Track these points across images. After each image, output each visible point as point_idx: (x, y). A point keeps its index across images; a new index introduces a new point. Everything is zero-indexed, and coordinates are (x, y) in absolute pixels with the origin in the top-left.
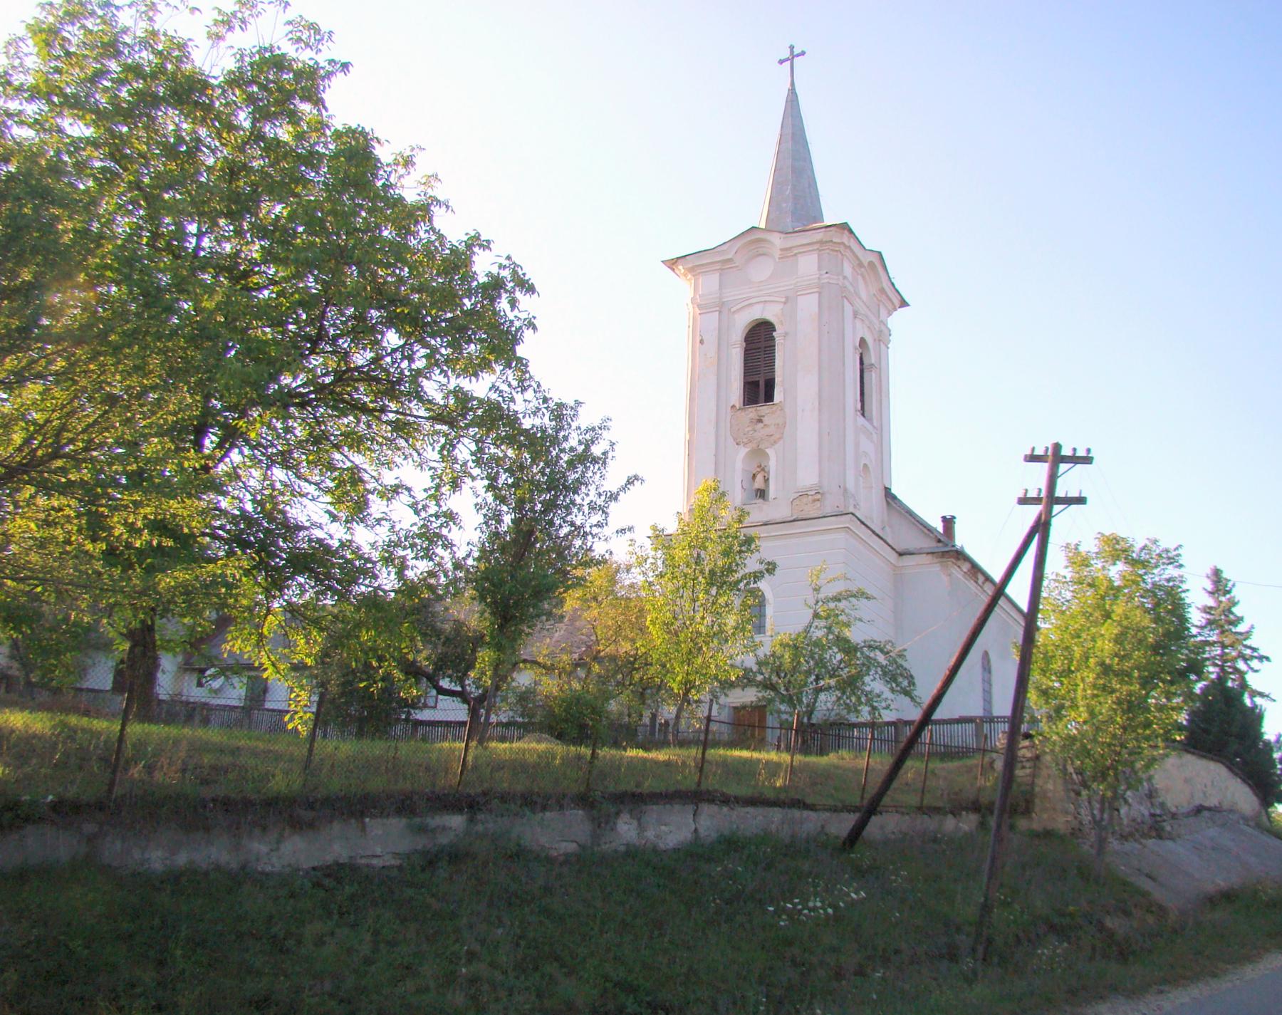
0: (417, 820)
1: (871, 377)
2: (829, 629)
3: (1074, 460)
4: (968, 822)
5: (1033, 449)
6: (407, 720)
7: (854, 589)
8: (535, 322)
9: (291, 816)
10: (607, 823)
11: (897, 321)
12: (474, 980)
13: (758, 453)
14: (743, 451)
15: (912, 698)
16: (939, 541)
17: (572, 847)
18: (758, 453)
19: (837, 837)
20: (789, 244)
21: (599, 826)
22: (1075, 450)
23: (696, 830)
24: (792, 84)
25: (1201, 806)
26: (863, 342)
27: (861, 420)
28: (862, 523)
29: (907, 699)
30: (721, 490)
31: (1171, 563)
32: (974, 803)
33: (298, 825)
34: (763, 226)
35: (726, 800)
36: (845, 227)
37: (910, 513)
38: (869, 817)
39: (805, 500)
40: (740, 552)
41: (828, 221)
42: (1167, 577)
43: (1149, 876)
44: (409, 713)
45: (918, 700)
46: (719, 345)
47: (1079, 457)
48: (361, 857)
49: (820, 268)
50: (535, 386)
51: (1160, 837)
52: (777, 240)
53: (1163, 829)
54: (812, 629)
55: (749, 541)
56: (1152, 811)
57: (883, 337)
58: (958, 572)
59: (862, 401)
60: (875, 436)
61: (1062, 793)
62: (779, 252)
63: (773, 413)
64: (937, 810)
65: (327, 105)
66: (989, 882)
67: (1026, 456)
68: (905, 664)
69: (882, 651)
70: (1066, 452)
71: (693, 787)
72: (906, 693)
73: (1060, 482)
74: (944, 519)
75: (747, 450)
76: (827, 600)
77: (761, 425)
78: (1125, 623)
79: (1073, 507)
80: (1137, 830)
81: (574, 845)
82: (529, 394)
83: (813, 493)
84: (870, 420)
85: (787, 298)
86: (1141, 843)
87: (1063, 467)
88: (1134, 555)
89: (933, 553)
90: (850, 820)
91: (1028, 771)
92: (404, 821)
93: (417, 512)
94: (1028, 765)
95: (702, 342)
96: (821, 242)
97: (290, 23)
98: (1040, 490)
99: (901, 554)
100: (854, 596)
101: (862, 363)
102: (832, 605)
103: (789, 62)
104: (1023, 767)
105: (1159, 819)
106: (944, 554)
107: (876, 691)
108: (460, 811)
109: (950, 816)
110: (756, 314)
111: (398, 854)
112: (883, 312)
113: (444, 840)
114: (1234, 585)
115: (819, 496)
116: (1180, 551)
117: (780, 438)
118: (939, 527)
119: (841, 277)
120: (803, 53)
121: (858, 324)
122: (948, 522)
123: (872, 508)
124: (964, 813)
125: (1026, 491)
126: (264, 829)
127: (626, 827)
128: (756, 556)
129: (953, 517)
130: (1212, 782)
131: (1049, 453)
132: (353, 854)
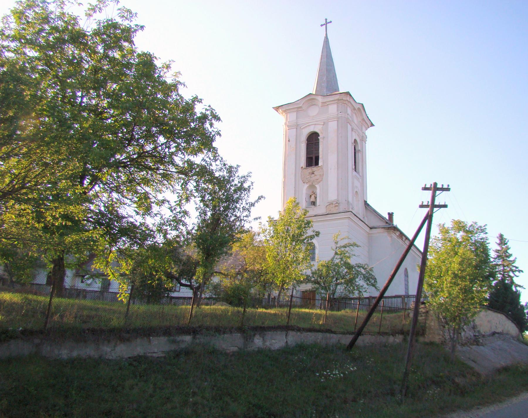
0: (172, 338)
1: (359, 155)
2: (342, 259)
3: (442, 189)
4: (399, 339)
5: (426, 185)
8: (221, 132)
9: (120, 336)
10: (250, 339)
12: (195, 404)
13: (312, 187)
14: (306, 186)
15: (376, 288)
16: (387, 223)
17: (235, 349)
18: (312, 187)
19: (345, 345)
20: (325, 100)
21: (247, 340)
22: (443, 185)
23: (287, 342)
24: (326, 34)
26: (355, 141)
27: (354, 173)
28: (355, 215)
29: (374, 288)
30: (297, 202)
31: (482, 232)
33: (123, 340)
34: (314, 93)
35: (299, 330)
36: (348, 94)
37: (375, 211)
38: (358, 337)
39: (331, 206)
40: (305, 227)
41: (341, 91)
42: (481, 237)
43: (473, 361)
45: (378, 288)
48: (149, 353)
49: (338, 111)
50: (220, 159)
51: (478, 345)
52: (320, 99)
53: (479, 341)
54: (335, 259)
55: (308, 223)
56: (475, 334)
57: (364, 139)
58: (395, 235)
60: (360, 179)
61: (438, 327)
66: (407, 363)
68: (373, 274)
69: (363, 268)
70: (439, 186)
71: (286, 324)
72: (373, 285)
73: (436, 198)
74: (389, 214)
75: (308, 185)
76: (341, 247)
77: (313, 175)
78: (463, 257)
79: (442, 209)
80: (468, 342)
81: (237, 348)
82: (218, 162)
83: (335, 203)
84: (358, 173)
86: (470, 347)
87: (438, 192)
88: (467, 229)
89: (384, 228)
90: (350, 338)
91: (423, 318)
93: (172, 211)
94: (423, 315)
95: (289, 141)
96: (338, 100)
98: (428, 202)
99: (371, 228)
102: (343, 249)
103: (325, 26)
104: (422, 316)
105: (477, 337)
106: (389, 228)
107: (361, 285)
108: (190, 334)
109: (391, 336)
110: (312, 129)
111: (164, 352)
112: (364, 128)
113: (183, 346)
114: (508, 241)
115: (337, 204)
116: (486, 227)
117: (321, 181)
118: (387, 217)
119: (346, 114)
120: (331, 22)
121: (354, 133)
122: (391, 215)
123: (359, 209)
124: (397, 335)
125: (423, 202)
127: (258, 341)
128: (311, 229)
129: (393, 213)
131: (432, 187)
132: (145, 352)
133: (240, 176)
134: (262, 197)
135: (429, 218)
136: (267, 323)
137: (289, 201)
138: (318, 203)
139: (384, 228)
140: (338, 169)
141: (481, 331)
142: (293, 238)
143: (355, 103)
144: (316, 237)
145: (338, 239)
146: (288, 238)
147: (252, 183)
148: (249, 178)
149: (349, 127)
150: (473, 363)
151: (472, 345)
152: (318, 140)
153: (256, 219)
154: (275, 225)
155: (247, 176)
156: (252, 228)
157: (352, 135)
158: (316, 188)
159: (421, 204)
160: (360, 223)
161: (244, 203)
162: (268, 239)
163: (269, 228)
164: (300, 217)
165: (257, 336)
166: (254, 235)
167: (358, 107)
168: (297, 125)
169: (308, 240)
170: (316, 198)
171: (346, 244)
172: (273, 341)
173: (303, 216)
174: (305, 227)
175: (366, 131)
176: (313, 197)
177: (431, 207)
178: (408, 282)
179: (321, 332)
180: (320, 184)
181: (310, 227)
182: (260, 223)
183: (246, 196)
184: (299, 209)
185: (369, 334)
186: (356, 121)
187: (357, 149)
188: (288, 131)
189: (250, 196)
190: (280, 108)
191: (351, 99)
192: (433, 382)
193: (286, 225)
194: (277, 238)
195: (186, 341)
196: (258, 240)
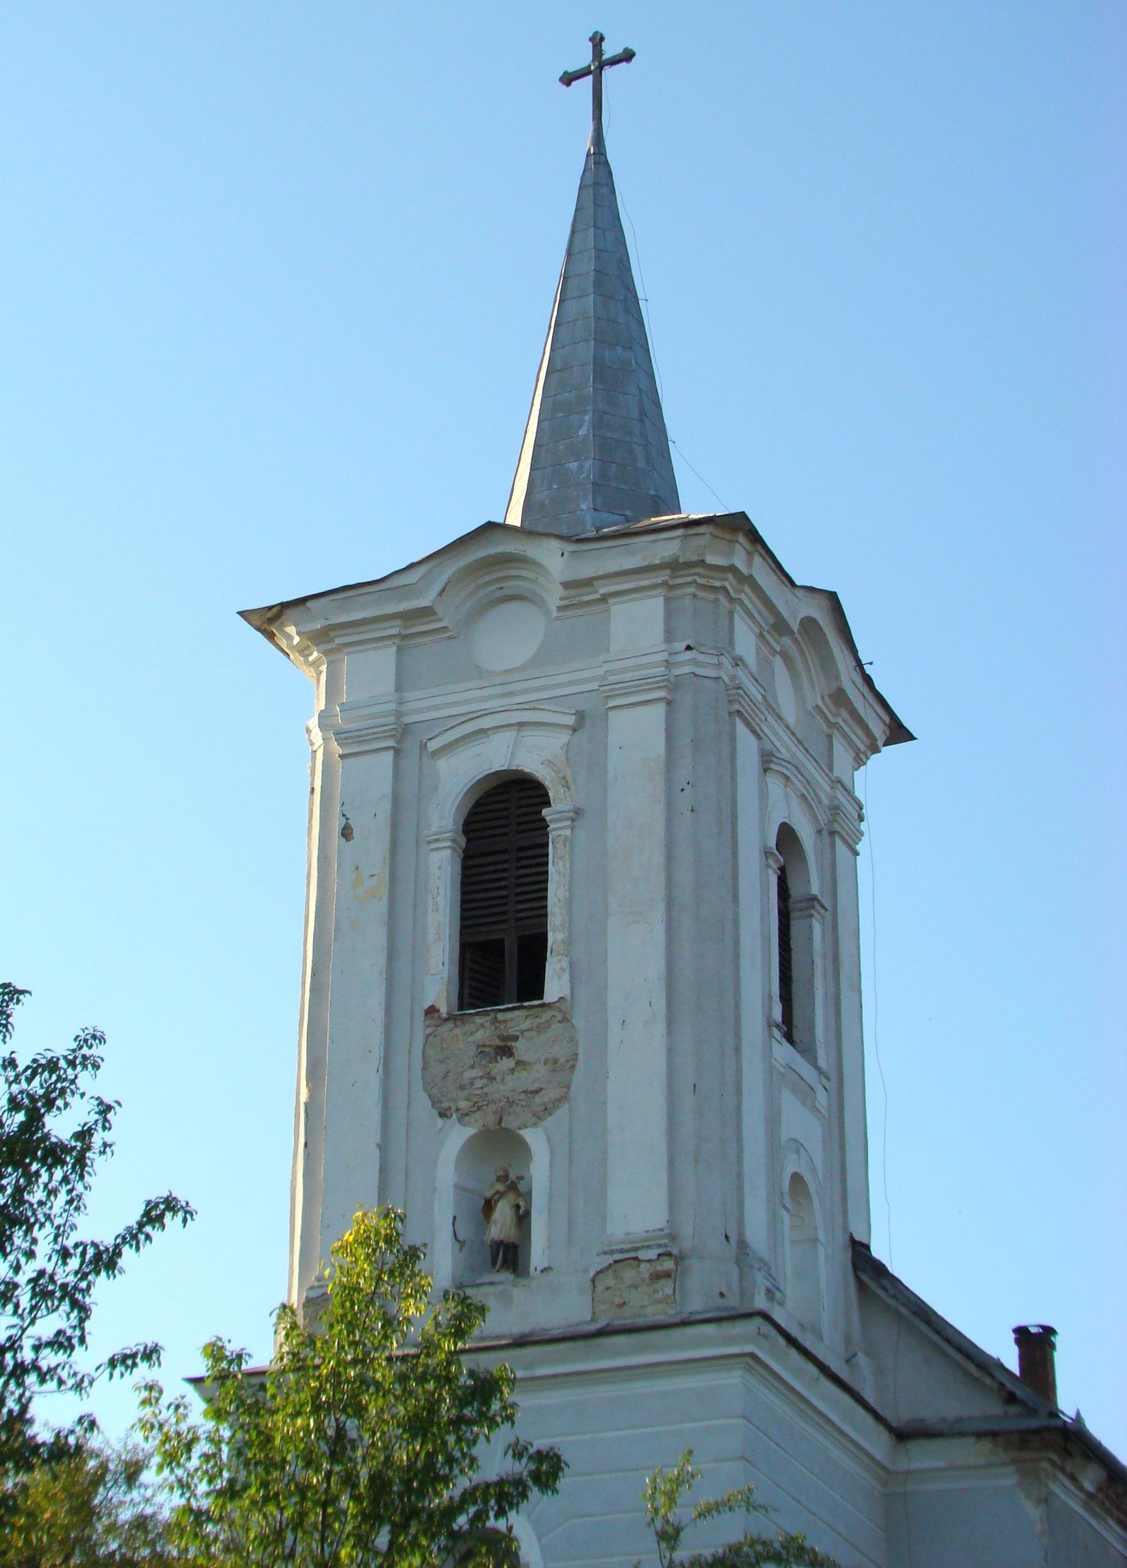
14: (458, 1135)
20: (587, 568)
26: (787, 836)
27: (783, 1051)
28: (792, 1341)
34: (514, 519)
39: (629, 1274)
40: (459, 1421)
41: (693, 508)
49: (669, 636)
60: (821, 1095)
62: (560, 591)
63: (540, 1029)
74: (1022, 1335)
75: (470, 1131)
77: (507, 1063)
83: (652, 1254)
84: (808, 1052)
85: (581, 716)
89: (993, 1435)
95: (346, 833)
96: (674, 566)
99: (902, 1435)
103: (589, 80)
112: (842, 755)
115: (668, 1264)
118: (1010, 1358)
119: (726, 661)
120: (628, 56)
121: (774, 785)
128: (503, 1435)
129: (1049, 1331)
133: (23, 1062)
134: (171, 1204)
137: (349, 1237)
138: (538, 1254)
139: (993, 1435)
140: (670, 1022)
142: (375, 1502)
143: (787, 591)
144: (534, 1493)
145: (683, 1513)
146: (345, 1501)
147: (105, 1109)
148: (84, 1079)
149: (747, 745)
152: (543, 825)
153: (123, 1361)
154: (255, 1409)
155: (72, 1063)
156: (93, 1424)
157: (763, 793)
158: (522, 1149)
160: (826, 1397)
161: (44, 1247)
162: (205, 1503)
163: (211, 1425)
164: (429, 1346)
166: (98, 1479)
167: (801, 615)
168: (403, 731)
169: (480, 1516)
170: (523, 1218)
173: (448, 1345)
174: (459, 1421)
175: (859, 775)
176: (503, 1211)
180: (549, 1121)
181: (493, 1423)
182: (150, 1388)
183: (63, 1197)
184: (420, 1290)
186: (789, 709)
187: (796, 890)
188: (340, 763)
189: (88, 1198)
190: (290, 613)
191: (757, 560)
193: (330, 1407)
194: (266, 1499)
196: (125, 1515)
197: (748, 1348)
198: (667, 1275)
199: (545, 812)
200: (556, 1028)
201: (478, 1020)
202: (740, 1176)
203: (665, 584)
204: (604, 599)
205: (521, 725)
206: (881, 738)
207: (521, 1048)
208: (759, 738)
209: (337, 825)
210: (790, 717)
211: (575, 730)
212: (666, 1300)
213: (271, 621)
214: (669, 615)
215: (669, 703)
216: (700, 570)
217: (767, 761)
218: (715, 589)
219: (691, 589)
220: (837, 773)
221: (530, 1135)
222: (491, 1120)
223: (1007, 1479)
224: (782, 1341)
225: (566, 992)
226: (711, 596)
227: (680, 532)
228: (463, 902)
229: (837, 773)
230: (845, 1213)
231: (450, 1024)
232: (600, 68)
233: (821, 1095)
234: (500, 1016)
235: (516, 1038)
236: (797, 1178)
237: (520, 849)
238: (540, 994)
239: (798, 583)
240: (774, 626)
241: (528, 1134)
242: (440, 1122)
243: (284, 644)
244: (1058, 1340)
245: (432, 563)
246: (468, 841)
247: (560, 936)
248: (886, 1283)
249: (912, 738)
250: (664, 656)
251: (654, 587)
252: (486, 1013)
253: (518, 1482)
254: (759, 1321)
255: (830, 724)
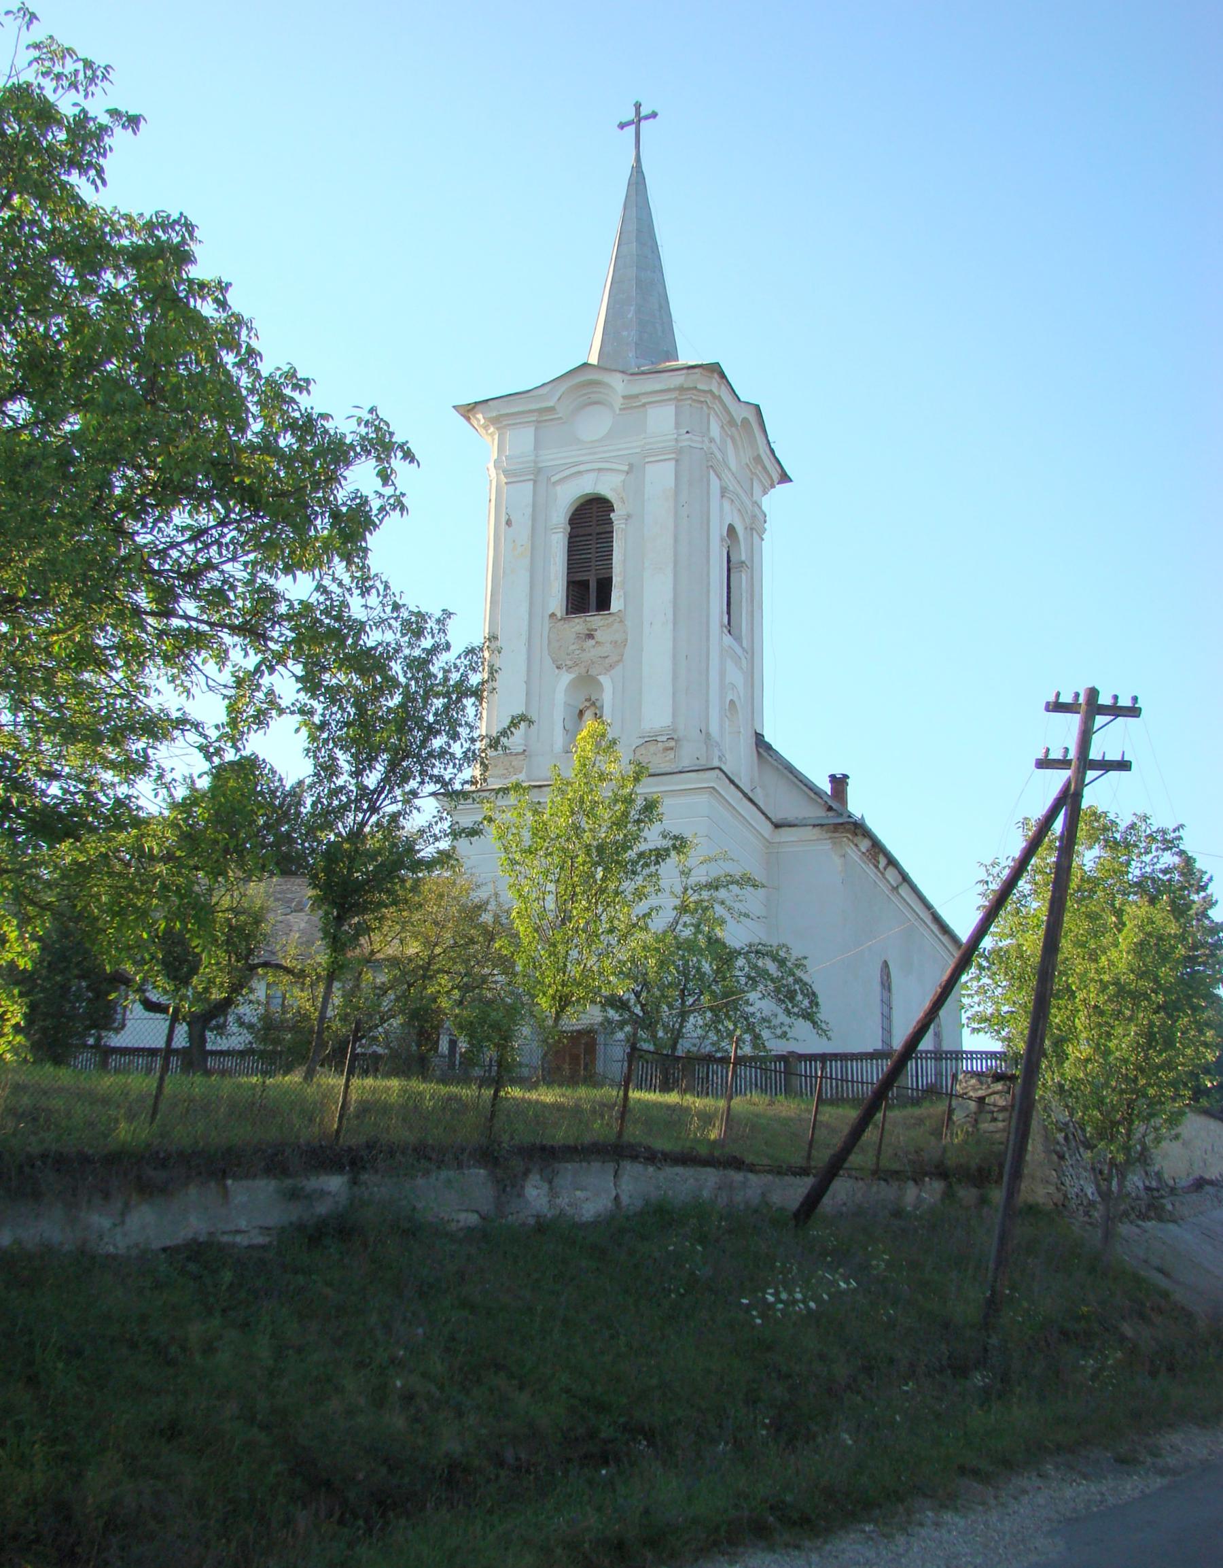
0: (289, 1182)
1: (741, 579)
2: (697, 926)
3: (1115, 711)
4: (933, 1190)
5: (1058, 695)
6: (96, 1046)
7: (737, 871)
8: (404, 500)
9: (139, 1178)
10: (513, 1186)
11: (775, 501)
12: (408, 1397)
13: (587, 681)
14: (566, 678)
15: (814, 1023)
16: (830, 809)
17: (473, 1219)
18: (587, 681)
19: (782, 1209)
20: (635, 389)
21: (504, 1191)
22: (1116, 697)
23: (617, 1197)
24: (638, 159)
25: (1201, 1178)
26: (731, 530)
27: (728, 639)
28: (732, 782)
29: (808, 1024)
30: (610, 736)
31: (1170, 848)
32: (937, 1167)
33: (147, 1190)
34: (594, 360)
35: (652, 1157)
36: (715, 370)
37: (790, 769)
38: (830, 1181)
39: (652, 748)
40: (638, 821)
41: (686, 358)
42: (1163, 867)
43: (1161, 1270)
44: (99, 1038)
45: (824, 1026)
46: (533, 529)
47: (1121, 708)
48: (224, 1233)
49: (677, 425)
50: (381, 588)
51: (1160, 1219)
52: (618, 384)
53: (1163, 1207)
54: (679, 927)
55: (650, 807)
56: (1147, 1183)
57: (757, 523)
58: (855, 852)
59: (729, 613)
60: (744, 661)
61: (1043, 1155)
62: (621, 400)
63: (609, 626)
64: (896, 1175)
65: (106, 176)
66: (996, 1269)
67: (1048, 704)
68: (805, 978)
69: (774, 959)
70: (1104, 699)
71: (612, 1138)
72: (808, 1016)
73: (1096, 739)
74: (833, 778)
75: (572, 676)
76: (699, 888)
77: (592, 642)
78: (1149, 929)
79: (1112, 774)
80: (1133, 1208)
81: (476, 1216)
82: (373, 600)
83: (664, 738)
84: (738, 639)
85: (631, 466)
86: (1138, 1226)
87: (1100, 720)
88: (1118, 836)
89: (822, 825)
90: (800, 1188)
91: (1000, 1125)
92: (273, 1183)
93: (208, 757)
94: (1000, 1116)
95: (509, 523)
96: (681, 389)
97: (37, 46)
98: (1066, 750)
99: (777, 826)
100: (737, 883)
101: (729, 561)
102: (705, 894)
103: (633, 127)
104: (994, 1120)
105: (1156, 1194)
106: (836, 827)
107: (766, 1013)
108: (340, 1169)
109: (911, 1184)
110: (587, 486)
111: (268, 1229)
112: (757, 489)
113: (322, 1209)
114: (1210, 879)
115: (672, 744)
116: (1182, 833)
117: (618, 661)
118: (826, 787)
119: (706, 439)
120: (654, 115)
121: (727, 505)
122: (839, 783)
123: (740, 761)
124: (927, 1179)
125: (1048, 750)
126: (107, 1196)
127: (535, 1192)
128: (657, 828)
129: (846, 777)
130: (1213, 1146)
131: (1081, 700)
132: (213, 1230)
135: (1069, 801)
136: (561, 1135)
140: (675, 623)
141: (1166, 1176)
150: (1161, 1275)
151: (1143, 1220)
159: (1041, 756)
165: (534, 1178)
168: (538, 471)
171: (717, 879)
172: (578, 1193)
177: (1078, 768)
178: (891, 1008)
179: (714, 1166)
180: (613, 672)
185: (850, 1176)
188: (506, 487)
190: (480, 407)
191: (723, 387)
192: (1064, 1333)
195: (329, 1193)
197: (712, 785)
198: (672, 749)
199: (612, 515)
200: (616, 625)
201: (577, 620)
202: (707, 701)
203: (676, 398)
204: (644, 405)
205: (600, 470)
206: (776, 481)
207: (598, 634)
208: (720, 480)
209: (504, 519)
210: (733, 468)
211: (628, 473)
212: (669, 761)
213: (469, 411)
214: (677, 414)
215: (677, 461)
216: (695, 392)
217: (724, 491)
218: (702, 402)
219: (689, 402)
220: (755, 498)
221: (602, 679)
222: (583, 671)
223: (827, 846)
224: (727, 781)
225: (622, 607)
226: (699, 406)
227: (684, 372)
228: (568, 560)
229: (755, 498)
230: (753, 719)
231: (562, 622)
232: (639, 121)
233: (744, 661)
234: (588, 619)
235: (596, 630)
236: (732, 702)
237: (598, 534)
238: (609, 609)
239: (742, 399)
240: (729, 422)
241: (601, 678)
242: (557, 671)
243: (475, 423)
244: (849, 781)
245: (555, 383)
246: (572, 528)
247: (619, 579)
248: (771, 753)
249: (791, 481)
250: (675, 436)
251: (669, 400)
252: (580, 617)
253: (667, 850)
254: (717, 771)
255: (753, 473)
